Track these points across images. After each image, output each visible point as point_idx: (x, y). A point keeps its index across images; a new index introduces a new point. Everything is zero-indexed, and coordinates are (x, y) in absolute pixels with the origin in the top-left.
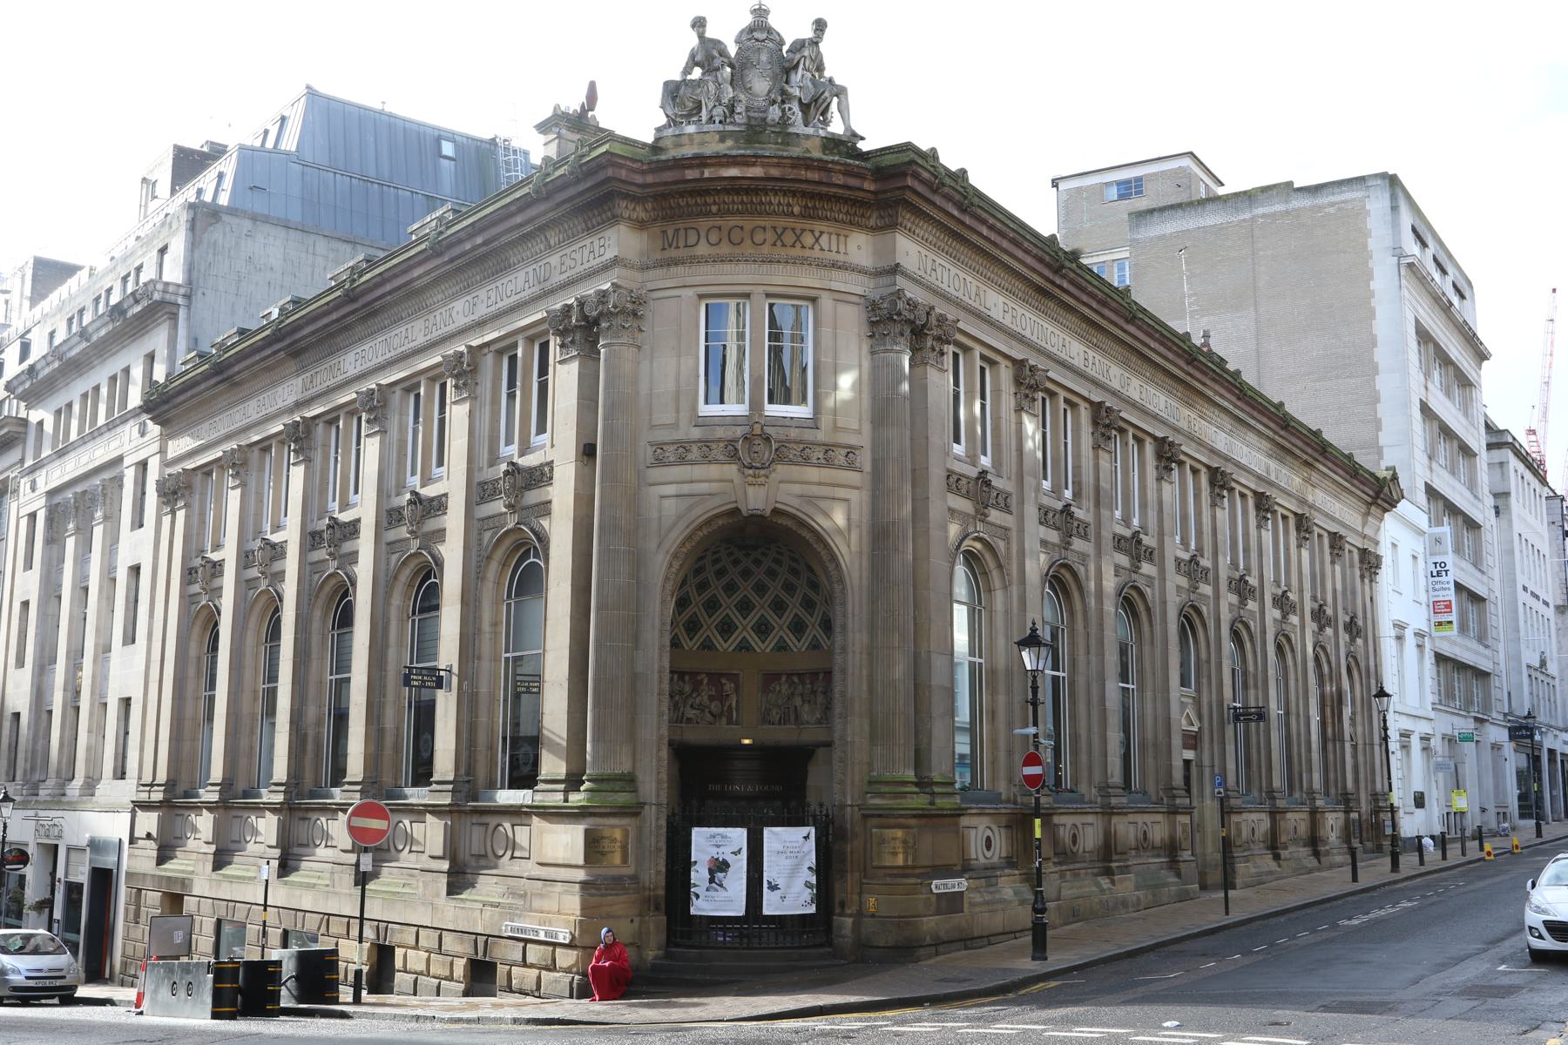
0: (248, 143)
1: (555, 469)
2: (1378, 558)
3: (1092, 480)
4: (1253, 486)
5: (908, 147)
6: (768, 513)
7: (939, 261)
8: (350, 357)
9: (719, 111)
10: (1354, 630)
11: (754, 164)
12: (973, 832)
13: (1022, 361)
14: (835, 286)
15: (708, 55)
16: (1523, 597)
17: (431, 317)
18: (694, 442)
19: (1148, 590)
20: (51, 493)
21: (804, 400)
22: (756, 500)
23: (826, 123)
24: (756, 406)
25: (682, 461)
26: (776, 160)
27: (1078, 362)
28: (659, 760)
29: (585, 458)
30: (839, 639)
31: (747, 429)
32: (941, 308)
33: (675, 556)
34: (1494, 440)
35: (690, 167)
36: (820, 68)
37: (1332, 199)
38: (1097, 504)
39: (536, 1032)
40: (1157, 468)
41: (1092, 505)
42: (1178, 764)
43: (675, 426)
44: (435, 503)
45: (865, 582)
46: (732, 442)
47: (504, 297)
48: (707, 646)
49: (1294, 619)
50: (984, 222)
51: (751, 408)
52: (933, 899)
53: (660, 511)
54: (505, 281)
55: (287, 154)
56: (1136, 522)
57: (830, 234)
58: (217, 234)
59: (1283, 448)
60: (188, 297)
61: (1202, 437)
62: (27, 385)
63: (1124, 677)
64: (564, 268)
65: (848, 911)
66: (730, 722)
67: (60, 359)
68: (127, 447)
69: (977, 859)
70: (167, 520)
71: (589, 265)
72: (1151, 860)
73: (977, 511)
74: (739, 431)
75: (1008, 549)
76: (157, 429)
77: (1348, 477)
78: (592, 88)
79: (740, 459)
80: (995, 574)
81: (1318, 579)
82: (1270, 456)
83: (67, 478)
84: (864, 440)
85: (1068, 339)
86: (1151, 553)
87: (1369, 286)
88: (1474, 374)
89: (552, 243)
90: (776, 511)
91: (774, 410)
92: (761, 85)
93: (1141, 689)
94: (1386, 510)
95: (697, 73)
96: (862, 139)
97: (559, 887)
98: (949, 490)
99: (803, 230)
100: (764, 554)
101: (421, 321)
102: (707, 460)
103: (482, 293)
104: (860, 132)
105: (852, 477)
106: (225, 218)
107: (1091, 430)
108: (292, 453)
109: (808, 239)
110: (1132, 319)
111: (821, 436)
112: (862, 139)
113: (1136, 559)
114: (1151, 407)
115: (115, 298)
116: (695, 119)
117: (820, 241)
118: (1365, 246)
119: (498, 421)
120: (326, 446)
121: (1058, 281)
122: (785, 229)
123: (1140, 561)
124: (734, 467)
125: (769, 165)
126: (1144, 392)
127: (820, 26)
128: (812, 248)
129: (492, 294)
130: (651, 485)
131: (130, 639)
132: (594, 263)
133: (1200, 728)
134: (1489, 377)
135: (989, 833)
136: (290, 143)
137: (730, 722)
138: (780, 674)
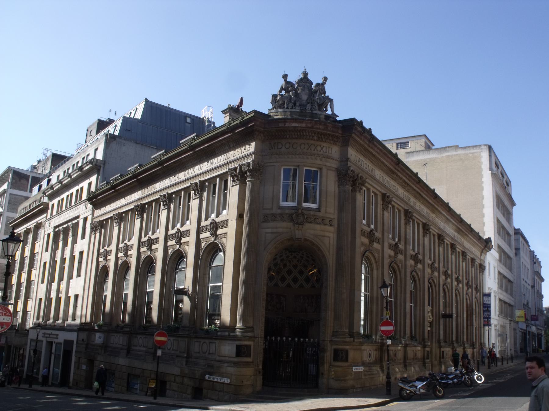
0: (126, 116)
1: (229, 222)
2: (485, 267)
5: (353, 120)
7: (361, 158)
9: (290, 105)
11: (302, 123)
14: (328, 164)
15: (288, 86)
16: (523, 282)
20: (55, 227)
23: (326, 110)
24: (299, 203)
25: (274, 221)
29: (240, 218)
34: (516, 232)
36: (325, 93)
38: (406, 243)
42: (426, 331)
43: (272, 209)
44: (185, 233)
45: (334, 265)
47: (213, 164)
49: (436, 274)
51: (298, 204)
52: (353, 373)
55: (138, 120)
56: (416, 250)
58: (114, 145)
59: (459, 229)
60: (104, 164)
64: (235, 155)
68: (81, 213)
70: (413, 332)
71: (244, 154)
74: (293, 211)
76: (91, 206)
78: (242, 99)
79: (294, 221)
81: (467, 273)
83: (61, 222)
84: (335, 217)
85: (398, 188)
86: (421, 261)
87: (482, 180)
88: (511, 210)
89: (231, 146)
91: (305, 205)
93: (416, 306)
95: (283, 92)
96: (338, 116)
97: (226, 365)
98: (362, 235)
99: (317, 145)
100: (297, 255)
104: (337, 114)
105: (331, 229)
106: (118, 139)
108: (136, 215)
109: (319, 148)
111: (321, 214)
112: (338, 116)
115: (80, 165)
116: (282, 107)
118: (480, 167)
122: (312, 144)
127: (325, 79)
131: (79, 275)
132: (245, 153)
133: (432, 320)
134: (515, 211)
135: (370, 352)
136: (139, 116)
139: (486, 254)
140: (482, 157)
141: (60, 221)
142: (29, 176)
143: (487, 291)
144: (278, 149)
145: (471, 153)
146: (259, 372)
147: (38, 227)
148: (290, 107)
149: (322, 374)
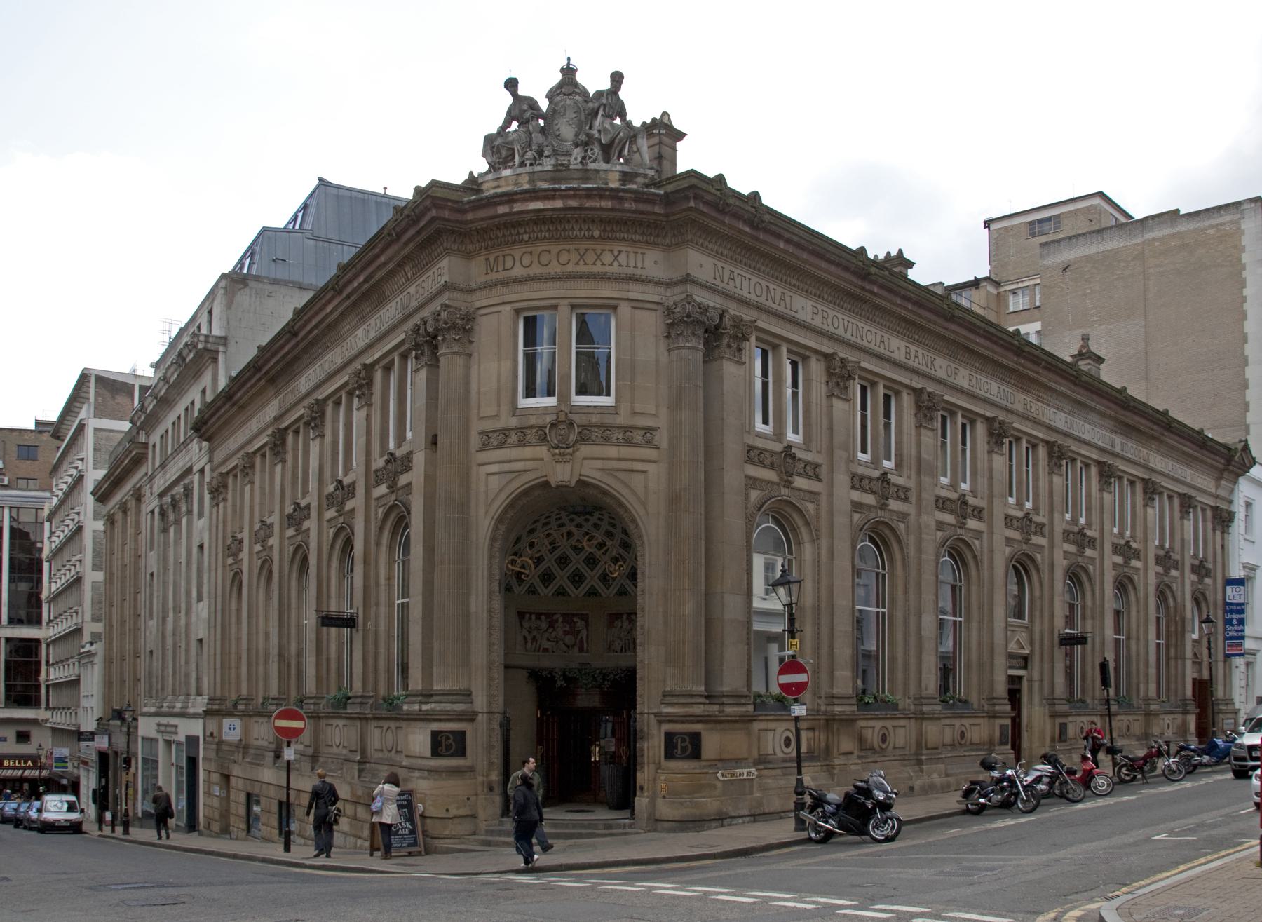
3: (914, 452)
4: (1095, 457)
6: (573, 484)
7: (737, 271)
8: (303, 380)
9: (529, 155)
10: (1203, 572)
11: (553, 198)
12: (770, 734)
13: (832, 354)
14: (632, 295)
15: (522, 109)
17: (344, 344)
18: (512, 429)
19: (976, 542)
20: (161, 495)
21: (608, 394)
22: (562, 474)
25: (503, 444)
26: (571, 192)
27: (899, 356)
28: (490, 679)
30: (640, 584)
31: (554, 417)
32: (734, 310)
33: (500, 520)
35: (501, 203)
37: (1212, 222)
38: (919, 472)
39: (802, 851)
40: (988, 443)
41: (913, 473)
43: (497, 416)
46: (542, 427)
48: (532, 591)
50: (779, 237)
51: (559, 401)
53: (487, 486)
54: (384, 310)
57: (636, 253)
61: (1040, 417)
62: (143, 418)
63: (405, 607)
65: (646, 794)
66: (581, 650)
67: (156, 398)
69: (775, 754)
72: (967, 754)
73: (781, 479)
74: (548, 419)
75: (817, 511)
77: (1198, 449)
80: (803, 530)
82: (1115, 432)
84: (662, 422)
87: (1242, 292)
90: (580, 482)
92: (567, 130)
93: (968, 621)
94: (1238, 475)
97: (417, 774)
101: (339, 348)
102: (522, 443)
103: (372, 321)
106: (252, 284)
107: (913, 412)
110: (951, 318)
111: (620, 420)
113: (1081, 547)
114: (982, 393)
116: (511, 164)
117: (619, 258)
118: (1239, 259)
119: (387, 422)
120: (295, 449)
121: (868, 287)
123: (965, 518)
124: (545, 448)
125: (568, 197)
126: (974, 380)
127: (617, 78)
128: (611, 265)
129: (378, 321)
130: (479, 465)
137: (581, 650)
138: (621, 615)
139: (1235, 482)
140: (1243, 233)
141: (166, 482)
142: (133, 385)
143: (1236, 572)
144: (504, 270)
145: (1212, 227)
146: (491, 789)
147: (138, 496)
148: (528, 163)
149: (642, 788)
